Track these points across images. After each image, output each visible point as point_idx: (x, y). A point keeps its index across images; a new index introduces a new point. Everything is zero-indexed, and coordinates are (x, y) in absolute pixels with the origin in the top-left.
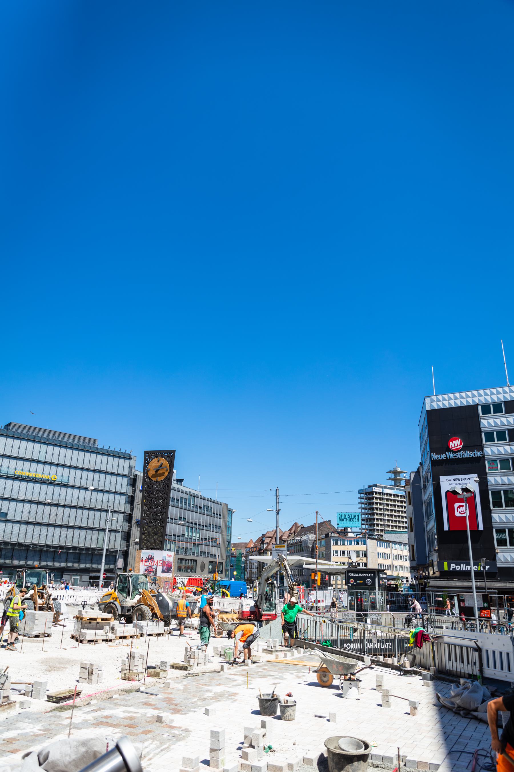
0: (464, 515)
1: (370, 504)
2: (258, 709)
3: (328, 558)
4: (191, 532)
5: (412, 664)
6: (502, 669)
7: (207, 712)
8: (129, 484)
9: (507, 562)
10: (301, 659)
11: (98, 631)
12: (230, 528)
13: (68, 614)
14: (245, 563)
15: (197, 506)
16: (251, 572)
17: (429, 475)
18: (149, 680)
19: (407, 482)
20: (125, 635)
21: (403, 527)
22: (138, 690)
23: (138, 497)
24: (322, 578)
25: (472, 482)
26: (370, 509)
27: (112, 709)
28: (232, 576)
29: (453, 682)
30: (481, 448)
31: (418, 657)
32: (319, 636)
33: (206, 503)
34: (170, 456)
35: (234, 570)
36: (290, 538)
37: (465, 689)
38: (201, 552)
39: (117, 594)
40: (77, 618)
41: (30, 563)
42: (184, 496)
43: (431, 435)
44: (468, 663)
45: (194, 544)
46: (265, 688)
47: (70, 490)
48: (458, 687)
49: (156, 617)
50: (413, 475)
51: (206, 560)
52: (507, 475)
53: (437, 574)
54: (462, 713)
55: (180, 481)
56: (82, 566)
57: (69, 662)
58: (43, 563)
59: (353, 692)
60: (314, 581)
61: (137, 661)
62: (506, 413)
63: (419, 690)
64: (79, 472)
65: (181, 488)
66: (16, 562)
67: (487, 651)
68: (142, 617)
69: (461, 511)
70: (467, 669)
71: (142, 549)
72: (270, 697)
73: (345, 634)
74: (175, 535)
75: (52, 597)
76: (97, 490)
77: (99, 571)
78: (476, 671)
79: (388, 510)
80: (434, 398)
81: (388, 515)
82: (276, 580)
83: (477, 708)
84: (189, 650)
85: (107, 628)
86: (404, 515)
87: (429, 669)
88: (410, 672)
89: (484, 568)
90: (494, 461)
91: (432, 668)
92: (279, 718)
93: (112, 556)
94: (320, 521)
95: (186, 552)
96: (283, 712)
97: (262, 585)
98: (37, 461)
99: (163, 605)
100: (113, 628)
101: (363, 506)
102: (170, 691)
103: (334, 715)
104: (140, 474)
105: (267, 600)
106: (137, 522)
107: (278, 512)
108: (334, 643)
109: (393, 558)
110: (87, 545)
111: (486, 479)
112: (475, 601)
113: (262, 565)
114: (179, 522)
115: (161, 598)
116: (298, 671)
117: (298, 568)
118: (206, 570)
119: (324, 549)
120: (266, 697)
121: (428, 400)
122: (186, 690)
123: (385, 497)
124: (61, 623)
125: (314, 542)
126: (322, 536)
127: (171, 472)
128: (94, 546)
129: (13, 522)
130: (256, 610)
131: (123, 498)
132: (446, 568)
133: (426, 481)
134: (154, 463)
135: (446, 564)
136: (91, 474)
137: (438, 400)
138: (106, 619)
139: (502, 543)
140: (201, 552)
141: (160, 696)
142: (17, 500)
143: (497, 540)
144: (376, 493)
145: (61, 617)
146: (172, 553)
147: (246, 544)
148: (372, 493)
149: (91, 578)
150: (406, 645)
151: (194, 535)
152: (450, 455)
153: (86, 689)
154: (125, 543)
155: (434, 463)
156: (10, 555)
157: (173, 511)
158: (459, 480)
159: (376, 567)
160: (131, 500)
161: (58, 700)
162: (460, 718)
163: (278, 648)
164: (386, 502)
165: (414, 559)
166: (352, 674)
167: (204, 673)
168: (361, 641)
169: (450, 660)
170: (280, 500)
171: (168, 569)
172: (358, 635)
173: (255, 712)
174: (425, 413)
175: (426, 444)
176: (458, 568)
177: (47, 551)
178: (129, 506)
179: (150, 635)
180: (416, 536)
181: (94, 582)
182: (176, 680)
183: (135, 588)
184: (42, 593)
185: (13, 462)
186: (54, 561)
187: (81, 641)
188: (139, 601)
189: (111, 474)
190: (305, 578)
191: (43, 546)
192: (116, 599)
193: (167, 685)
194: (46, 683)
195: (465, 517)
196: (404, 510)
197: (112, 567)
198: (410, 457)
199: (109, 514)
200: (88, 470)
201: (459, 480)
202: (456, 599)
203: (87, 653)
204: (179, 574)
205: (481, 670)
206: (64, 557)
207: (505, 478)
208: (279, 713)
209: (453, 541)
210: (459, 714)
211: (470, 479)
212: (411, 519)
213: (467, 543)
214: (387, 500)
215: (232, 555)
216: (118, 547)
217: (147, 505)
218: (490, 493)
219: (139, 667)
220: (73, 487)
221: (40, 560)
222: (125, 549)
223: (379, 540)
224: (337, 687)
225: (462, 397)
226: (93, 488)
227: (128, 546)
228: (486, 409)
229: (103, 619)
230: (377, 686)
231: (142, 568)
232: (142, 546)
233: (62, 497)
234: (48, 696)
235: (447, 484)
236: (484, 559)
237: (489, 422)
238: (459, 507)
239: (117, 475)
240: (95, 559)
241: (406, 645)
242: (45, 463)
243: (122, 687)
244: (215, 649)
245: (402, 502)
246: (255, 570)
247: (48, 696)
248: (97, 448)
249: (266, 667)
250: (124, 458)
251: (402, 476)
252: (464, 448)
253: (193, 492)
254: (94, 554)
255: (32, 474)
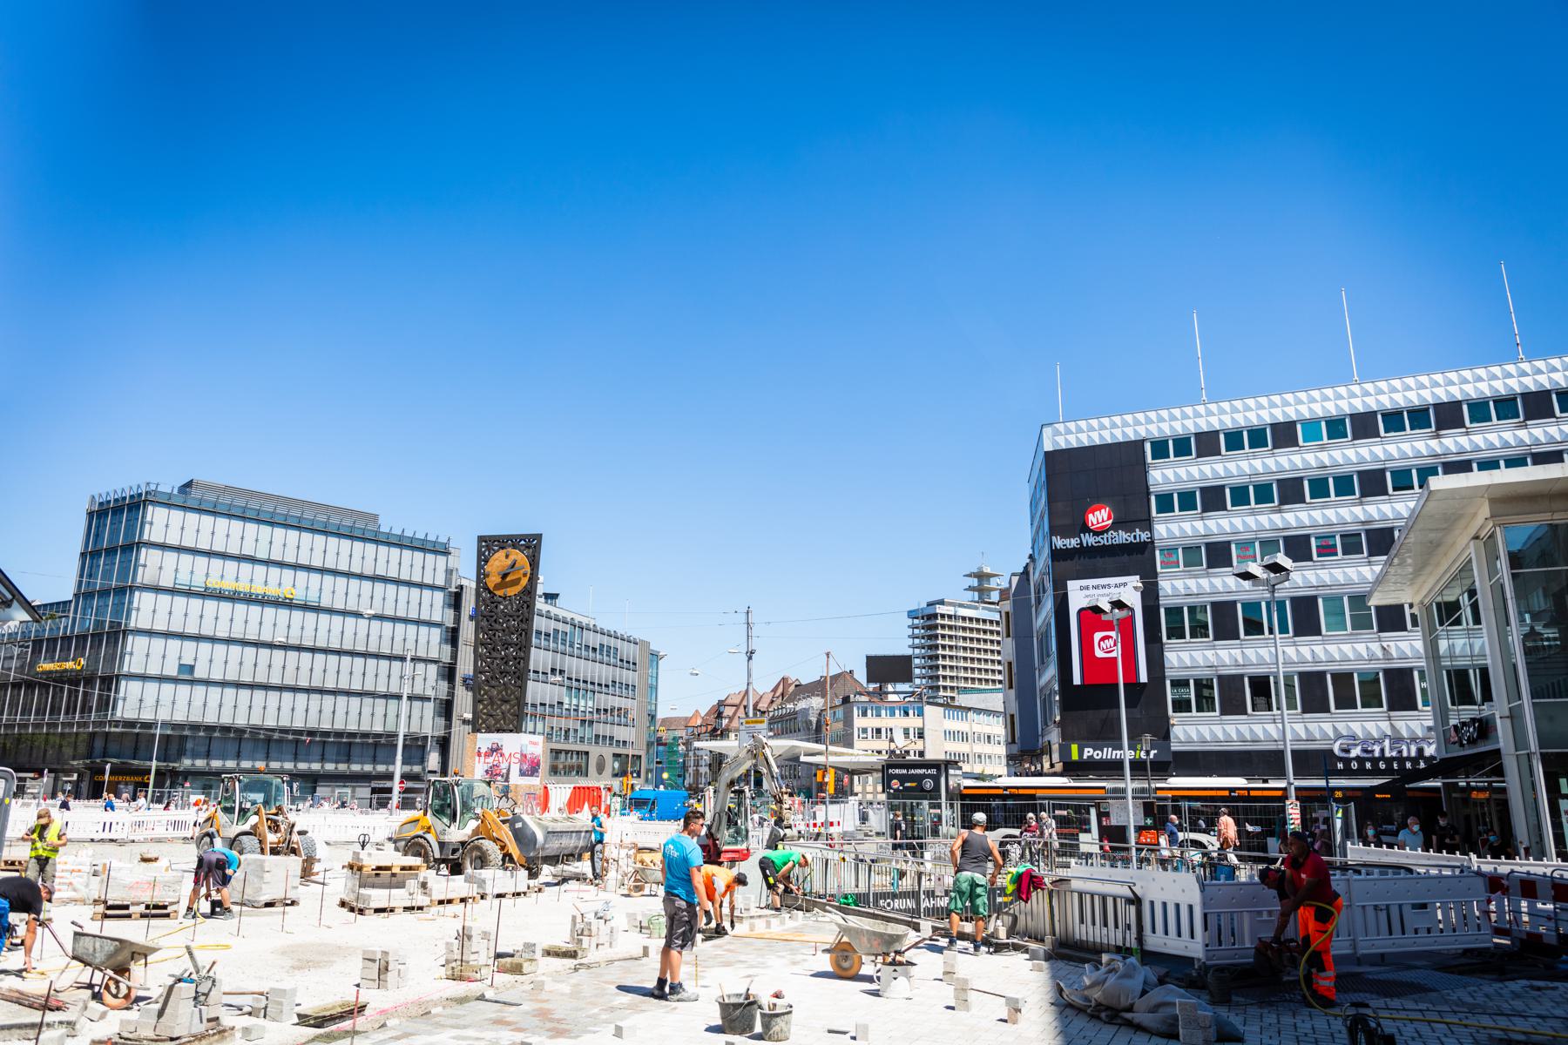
0: (1113, 655)
1: (930, 637)
2: (719, 1022)
3: (849, 744)
4: (577, 697)
5: (1011, 932)
6: (1179, 935)
7: (619, 1032)
8: (447, 605)
9: (1191, 742)
10: (798, 930)
11: (394, 891)
12: (654, 688)
13: (331, 862)
14: (686, 755)
15: (587, 647)
16: (697, 774)
17: (1046, 578)
18: (502, 978)
19: (1004, 594)
20: (449, 897)
21: (994, 681)
22: (482, 998)
23: (468, 631)
24: (838, 780)
25: (1129, 590)
26: (930, 647)
27: (430, 1033)
28: (659, 782)
29: (1088, 961)
30: (1148, 524)
31: (1022, 919)
32: (832, 888)
33: (606, 640)
34: (531, 545)
35: (663, 770)
36: (774, 706)
37: (1110, 971)
38: (597, 736)
39: (430, 819)
40: (351, 867)
41: (246, 764)
42: (561, 626)
43: (1051, 500)
44: (1116, 927)
45: (583, 722)
46: (733, 985)
47: (324, 617)
48: (1098, 969)
49: (512, 860)
50: (1015, 580)
51: (608, 751)
52: (1196, 577)
53: (1059, 767)
54: (1103, 1015)
55: (551, 597)
56: (356, 768)
57: (340, 951)
58: (275, 765)
59: (899, 986)
60: (822, 787)
61: (477, 944)
62: (1199, 456)
63: (1024, 978)
64: (341, 581)
65: (554, 611)
66: (216, 764)
67: (1152, 903)
68: (482, 861)
69: (1107, 646)
70: (1114, 936)
71: (479, 731)
72: (741, 1000)
73: (881, 882)
74: (543, 705)
75: (296, 829)
76: (380, 618)
77: (390, 777)
78: (1132, 942)
79: (965, 649)
80: (1060, 427)
81: (965, 659)
82: (748, 783)
83: (1132, 1005)
84: (579, 919)
85: (412, 884)
86: (996, 657)
87: (1042, 941)
88: (1006, 946)
89: (1148, 753)
90: (1170, 551)
91: (1048, 938)
92: (760, 1037)
93: (416, 748)
94: (834, 671)
95: (567, 737)
96: (767, 1026)
97: (721, 795)
98: (335, 573)
99: (523, 837)
100: (424, 885)
101: (917, 641)
102: (544, 996)
103: (864, 1029)
104: (470, 584)
105: (731, 822)
106: (465, 680)
107: (750, 655)
108: (861, 899)
109: (972, 738)
110: (365, 728)
111: (1156, 584)
112: (1129, 815)
113: (718, 760)
114: (552, 678)
115: (519, 825)
116: (793, 951)
117: (791, 762)
118: (608, 771)
119: (840, 725)
120: (734, 1000)
121: (1047, 432)
122: (576, 993)
123: (960, 624)
124: (319, 878)
125: (821, 713)
126: (838, 702)
127: (533, 579)
128: (378, 728)
129: (207, 683)
130: (710, 842)
131: (436, 633)
132: (1075, 757)
133: (1041, 589)
134: (499, 561)
135: (1074, 748)
136: (367, 585)
137: (1069, 432)
138: (411, 868)
139: (1182, 706)
140: (597, 736)
141: (525, 1007)
142: (213, 640)
143: (1174, 701)
144: (943, 616)
145: (317, 867)
146: (540, 739)
147: (686, 719)
148: (935, 616)
149: (374, 791)
150: (999, 900)
151: (582, 703)
152: (1089, 540)
153: (375, 999)
154: (441, 722)
155: (1057, 555)
156: (203, 749)
157: (539, 658)
158: (1104, 587)
159: (943, 757)
160: (453, 637)
161: (321, 1021)
162: (1099, 1025)
163: (754, 912)
164: (961, 633)
165: (1013, 741)
166: (897, 953)
167: (611, 962)
168: (914, 895)
169: (1082, 921)
170: (754, 632)
171: (532, 769)
172: (907, 884)
173: (711, 1029)
174: (1041, 457)
175: (1042, 517)
176: (1098, 755)
177: (280, 741)
178: (448, 648)
179: (500, 896)
180: (1019, 697)
181: (380, 798)
182: (556, 976)
183: (466, 807)
184: (275, 822)
185: (202, 561)
186: (296, 759)
187: (361, 912)
188: (476, 832)
189: (409, 584)
190: (804, 782)
191: (273, 730)
192: (428, 830)
193: (538, 987)
194: (294, 991)
195: (1115, 659)
196: (995, 647)
197: (417, 769)
198: (1010, 542)
199: (408, 665)
200: (361, 577)
201: (1104, 587)
202: (1093, 811)
203: (372, 933)
204: (554, 779)
205: (1140, 939)
206: (317, 750)
207: (1192, 583)
208: (758, 1029)
209: (1090, 704)
210: (1098, 1018)
211: (1125, 584)
212: (1010, 664)
213: (1118, 706)
214: (964, 629)
215: (660, 742)
216: (428, 730)
217: (487, 644)
218: (1162, 611)
219: (481, 954)
220: (331, 611)
221: (267, 758)
222: (442, 733)
223: (946, 706)
224: (869, 979)
225: (1114, 426)
226: (372, 612)
227: (449, 726)
228: (1160, 449)
229: (403, 868)
230: (946, 973)
231: (479, 769)
232: (476, 726)
233: (309, 632)
234: (299, 1016)
235: (1081, 594)
236: (1148, 737)
237: (1165, 475)
238: (1103, 639)
239: (421, 586)
240: (381, 753)
241: (999, 900)
242: (268, 563)
243: (448, 994)
244: (631, 916)
245: (992, 632)
246: (704, 770)
247: (299, 1016)
248: (377, 533)
249: (732, 947)
250: (436, 552)
251: (993, 583)
252: (1116, 526)
253: (578, 619)
254: (380, 745)
255: (243, 587)
